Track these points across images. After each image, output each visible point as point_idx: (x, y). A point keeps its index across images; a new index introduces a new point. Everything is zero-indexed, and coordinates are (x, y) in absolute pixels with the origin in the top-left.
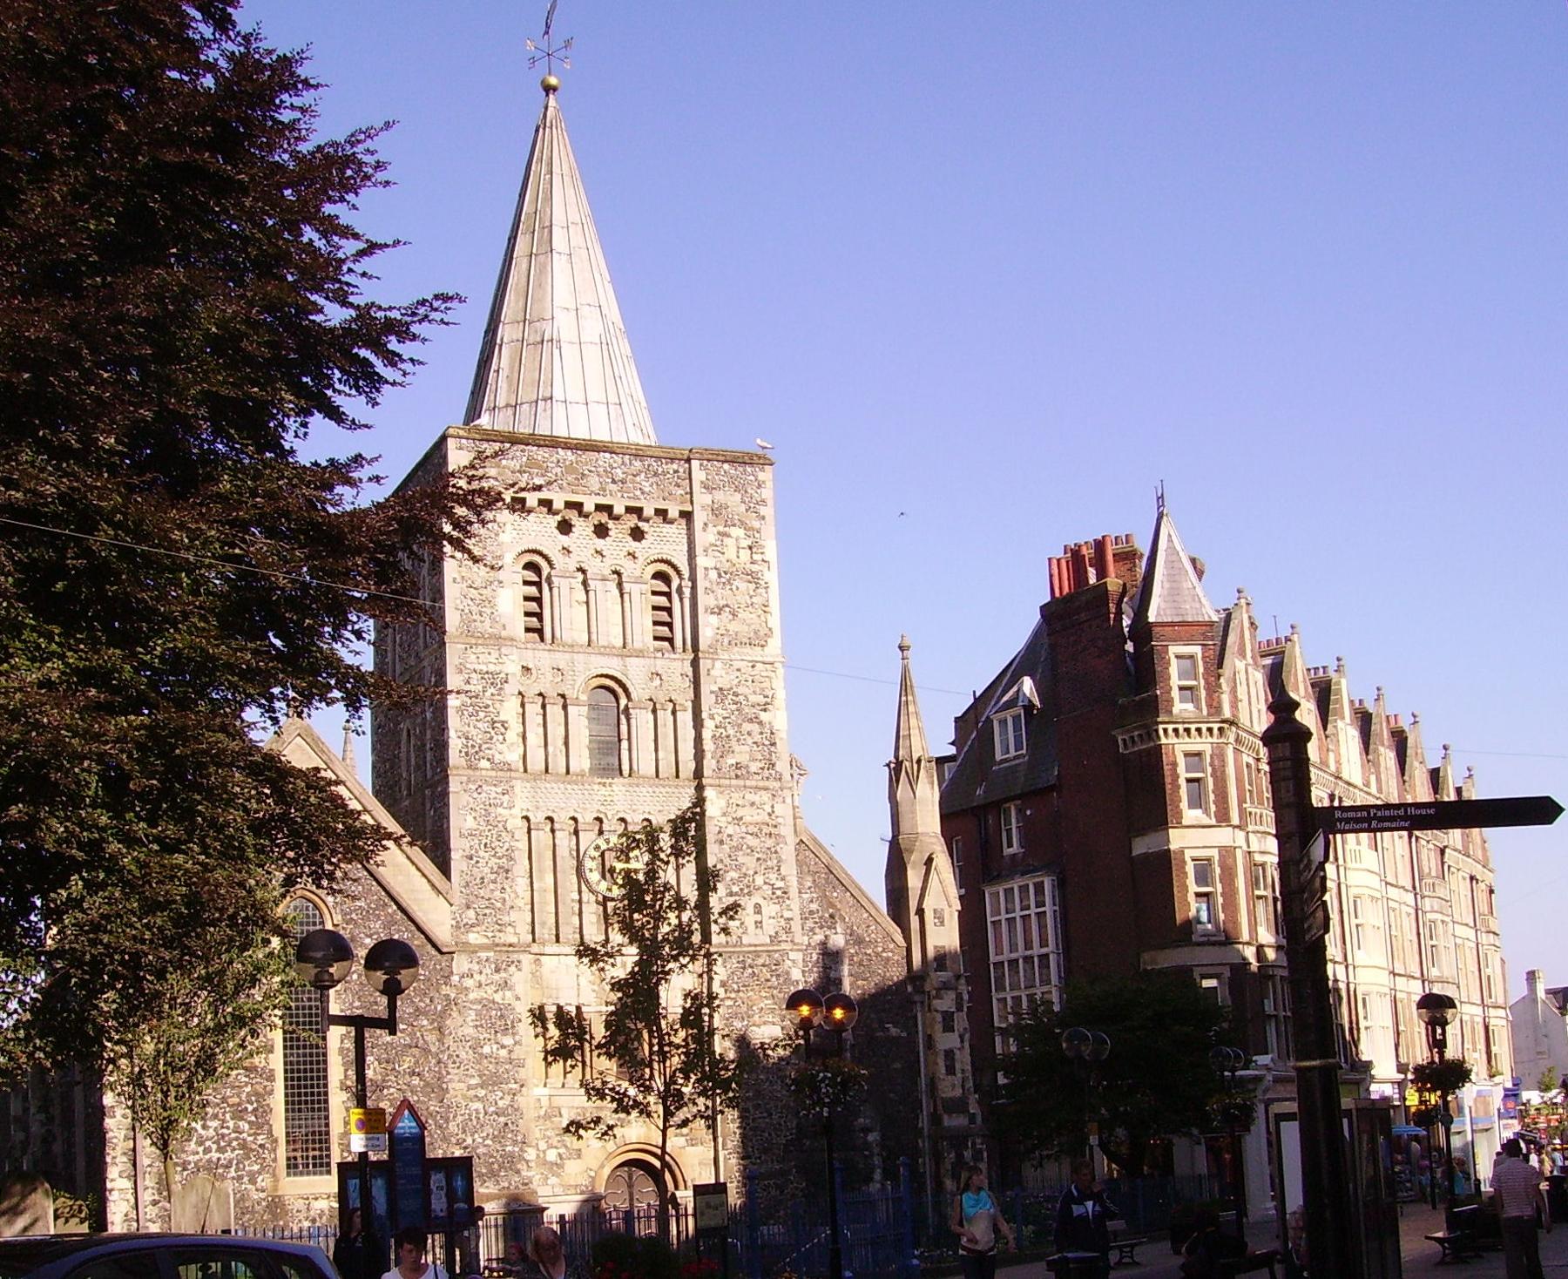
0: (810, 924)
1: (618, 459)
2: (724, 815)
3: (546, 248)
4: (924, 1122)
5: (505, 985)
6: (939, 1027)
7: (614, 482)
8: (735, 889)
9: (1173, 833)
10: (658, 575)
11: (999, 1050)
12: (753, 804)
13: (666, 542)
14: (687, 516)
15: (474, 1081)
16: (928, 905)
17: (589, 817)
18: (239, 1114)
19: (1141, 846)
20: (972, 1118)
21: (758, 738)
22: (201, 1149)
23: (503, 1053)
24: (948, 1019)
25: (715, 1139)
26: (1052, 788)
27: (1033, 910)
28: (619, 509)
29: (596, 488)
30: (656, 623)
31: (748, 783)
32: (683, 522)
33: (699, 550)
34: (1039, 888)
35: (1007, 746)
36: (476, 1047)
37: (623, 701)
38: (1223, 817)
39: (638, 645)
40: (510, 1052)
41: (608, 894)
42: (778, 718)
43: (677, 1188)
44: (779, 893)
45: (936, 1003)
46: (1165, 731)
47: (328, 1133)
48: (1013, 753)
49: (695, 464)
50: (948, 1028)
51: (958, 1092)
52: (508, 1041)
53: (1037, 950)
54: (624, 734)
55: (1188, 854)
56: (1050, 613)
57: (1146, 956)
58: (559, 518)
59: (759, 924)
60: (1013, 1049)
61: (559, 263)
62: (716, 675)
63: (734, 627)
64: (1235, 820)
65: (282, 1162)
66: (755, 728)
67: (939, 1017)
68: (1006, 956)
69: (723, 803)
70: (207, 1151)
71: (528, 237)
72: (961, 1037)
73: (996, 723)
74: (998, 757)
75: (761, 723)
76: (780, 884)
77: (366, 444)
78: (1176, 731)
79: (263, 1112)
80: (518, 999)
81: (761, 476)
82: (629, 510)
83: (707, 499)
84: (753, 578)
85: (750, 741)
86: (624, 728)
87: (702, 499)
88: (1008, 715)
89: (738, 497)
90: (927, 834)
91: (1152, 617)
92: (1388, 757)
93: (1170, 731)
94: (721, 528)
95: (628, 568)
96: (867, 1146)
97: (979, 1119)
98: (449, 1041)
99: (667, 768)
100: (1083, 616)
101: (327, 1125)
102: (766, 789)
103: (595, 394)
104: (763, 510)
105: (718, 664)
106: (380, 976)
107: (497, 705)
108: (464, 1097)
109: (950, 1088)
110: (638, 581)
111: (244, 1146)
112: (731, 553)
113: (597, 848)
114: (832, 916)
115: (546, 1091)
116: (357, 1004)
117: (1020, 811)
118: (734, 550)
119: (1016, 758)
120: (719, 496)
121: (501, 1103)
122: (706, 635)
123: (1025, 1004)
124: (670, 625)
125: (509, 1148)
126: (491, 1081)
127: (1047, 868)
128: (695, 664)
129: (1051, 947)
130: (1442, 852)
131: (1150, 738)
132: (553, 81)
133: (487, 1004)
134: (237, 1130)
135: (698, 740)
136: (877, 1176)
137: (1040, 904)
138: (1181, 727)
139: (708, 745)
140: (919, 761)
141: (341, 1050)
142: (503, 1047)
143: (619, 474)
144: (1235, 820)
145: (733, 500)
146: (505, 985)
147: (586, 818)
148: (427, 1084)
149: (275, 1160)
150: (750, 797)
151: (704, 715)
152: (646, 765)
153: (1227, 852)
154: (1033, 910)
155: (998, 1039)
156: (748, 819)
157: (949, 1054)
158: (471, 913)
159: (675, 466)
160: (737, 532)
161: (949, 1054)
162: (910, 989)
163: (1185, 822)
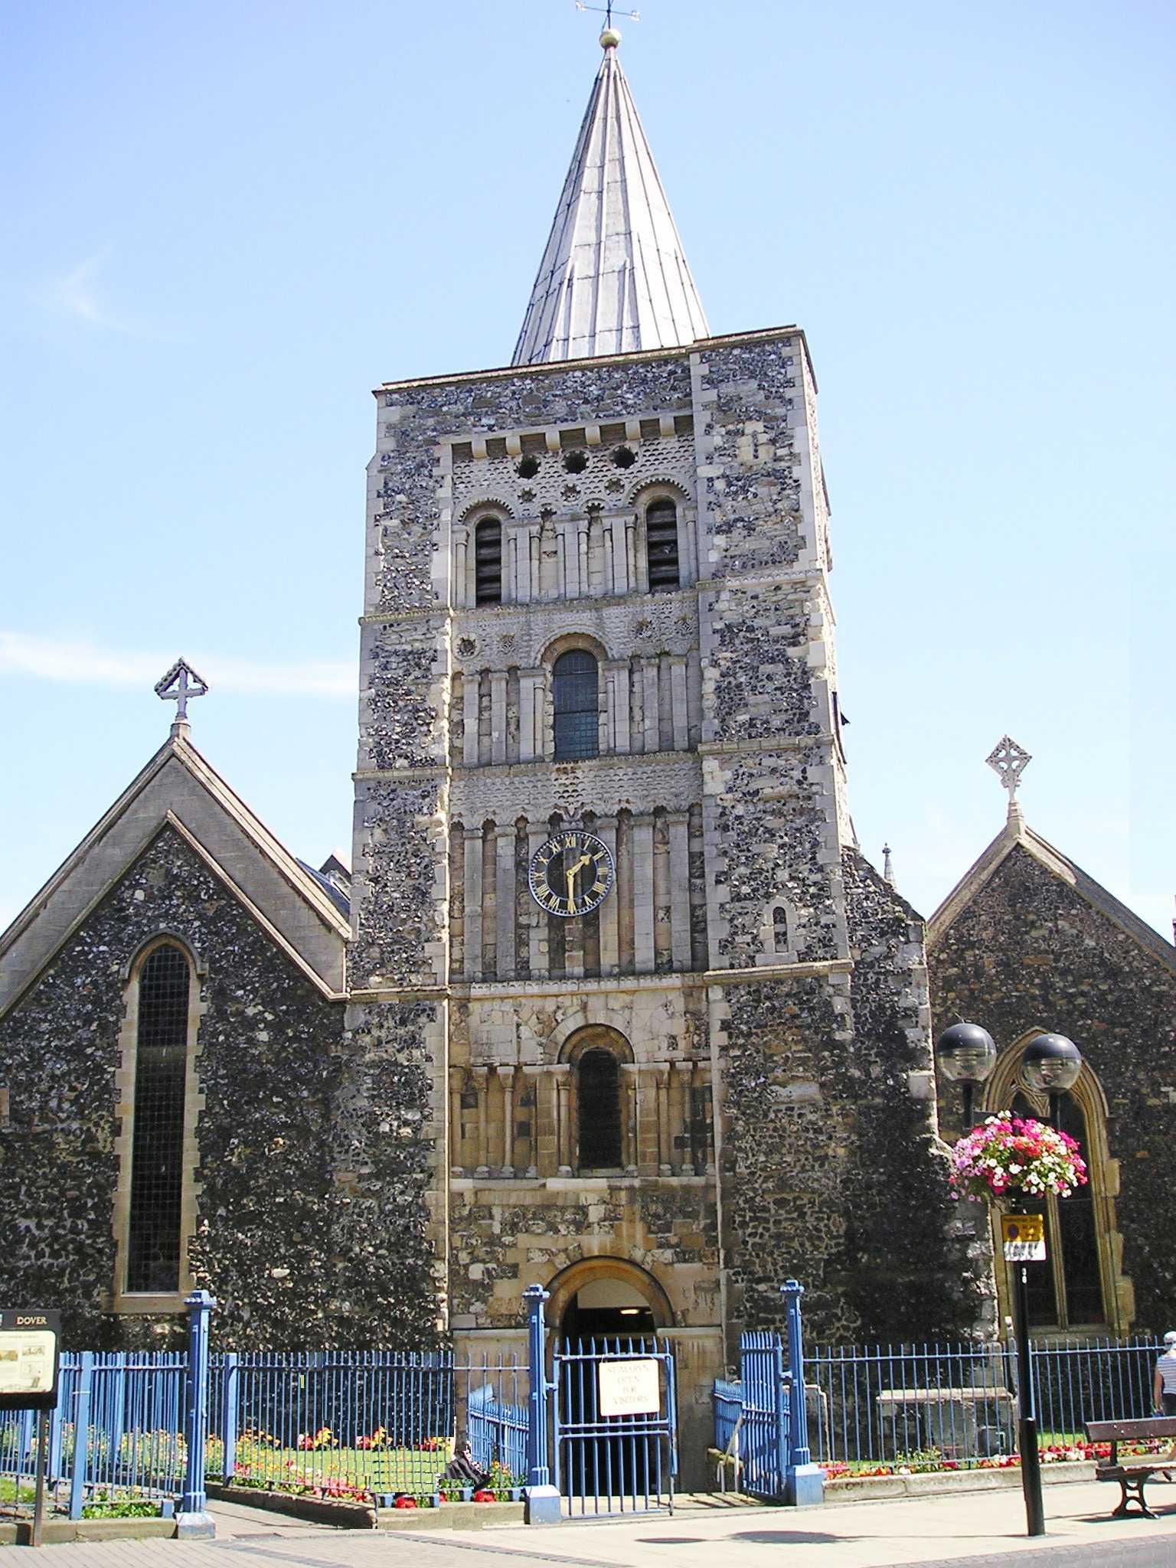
2: (730, 790)
5: (413, 1042)
7: (586, 402)
8: (745, 889)
12: (774, 770)
15: (365, 1170)
18: (78, 1212)
22: (33, 1254)
23: (406, 1131)
36: (373, 1121)
44: (812, 890)
59: (781, 937)
63: (748, 545)
66: (780, 668)
69: (729, 775)
70: (40, 1255)
75: (787, 661)
79: (105, 1207)
80: (429, 1059)
81: (786, 351)
83: (712, 395)
87: (703, 395)
89: (754, 384)
94: (731, 427)
98: (336, 1117)
104: (789, 393)
107: (423, 690)
108: (354, 1190)
112: (746, 453)
116: (222, 1072)
120: (728, 389)
125: (411, 1261)
126: (387, 1170)
131: (1085, 1196)
133: (388, 1067)
134: (74, 1230)
141: (199, 1132)
142: (406, 1123)
145: (748, 389)
146: (413, 1042)
147: (505, 818)
148: (304, 1174)
150: (768, 762)
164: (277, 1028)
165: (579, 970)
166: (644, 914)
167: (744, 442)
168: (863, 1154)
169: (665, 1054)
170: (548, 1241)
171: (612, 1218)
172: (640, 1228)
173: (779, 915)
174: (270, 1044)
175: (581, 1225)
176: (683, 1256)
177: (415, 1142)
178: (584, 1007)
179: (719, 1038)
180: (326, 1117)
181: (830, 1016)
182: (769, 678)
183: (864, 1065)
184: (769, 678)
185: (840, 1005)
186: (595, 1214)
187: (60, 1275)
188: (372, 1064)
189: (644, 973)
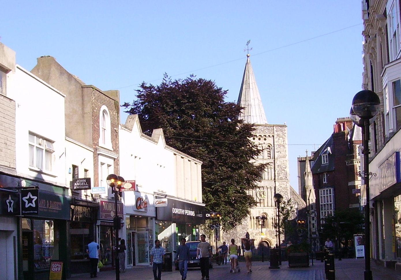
1: (262, 127)
2: (279, 186)
3: (248, 88)
4: (309, 236)
7: (262, 131)
9: (356, 182)
11: (321, 223)
13: (270, 141)
14: (273, 136)
19: (350, 184)
20: (317, 235)
21: (284, 173)
23: (245, 224)
24: (313, 218)
25: (277, 238)
26: (333, 171)
28: (262, 136)
29: (259, 132)
30: (268, 154)
31: (283, 181)
32: (272, 137)
33: (275, 142)
34: (330, 190)
35: (325, 161)
39: (265, 158)
40: (246, 224)
41: (261, 199)
42: (287, 170)
43: (271, 245)
45: (311, 215)
46: (355, 162)
47: (220, 236)
48: (325, 163)
49: (275, 127)
50: (313, 220)
51: (315, 231)
52: (246, 222)
53: (329, 203)
57: (350, 205)
60: (324, 223)
61: (251, 90)
62: (278, 163)
63: (280, 155)
65: (214, 240)
66: (284, 171)
67: (312, 218)
68: (323, 203)
71: (245, 85)
72: (315, 221)
73: (322, 157)
74: (323, 163)
75: (285, 171)
76: (287, 197)
77: (256, 161)
78: (357, 162)
81: (285, 129)
82: (264, 136)
83: (276, 133)
84: (284, 146)
85: (283, 173)
87: (276, 133)
88: (325, 155)
90: (310, 186)
91: (353, 140)
93: (356, 162)
94: (279, 138)
97: (318, 236)
99: (270, 178)
100: (340, 138)
101: (220, 235)
102: (285, 181)
103: (258, 114)
104: (285, 135)
109: (313, 230)
112: (280, 142)
113: (259, 191)
114: (296, 202)
115: (251, 230)
117: (326, 174)
118: (281, 142)
119: (326, 164)
120: (278, 133)
121: (245, 232)
124: (270, 154)
127: (331, 187)
129: (332, 202)
131: (352, 163)
132: (248, 55)
135: (275, 173)
137: (330, 193)
138: (358, 161)
139: (276, 174)
140: (309, 173)
143: (263, 130)
145: (280, 133)
149: (213, 240)
150: (283, 183)
151: (276, 170)
152: (266, 178)
154: (329, 195)
155: (321, 221)
156: (282, 186)
157: (313, 224)
159: (271, 128)
160: (281, 139)
161: (313, 224)
162: (307, 213)
163: (358, 180)
169: (272, 216)
172: (269, 235)
178: (263, 210)
182: (283, 172)
184: (283, 172)
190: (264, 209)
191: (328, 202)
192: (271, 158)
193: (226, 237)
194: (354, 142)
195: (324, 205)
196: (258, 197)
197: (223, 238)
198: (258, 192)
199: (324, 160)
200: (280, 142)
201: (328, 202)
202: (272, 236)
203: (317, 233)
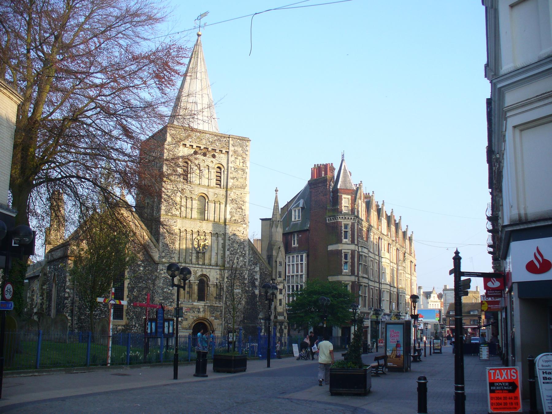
0: (251, 263)
6: (278, 293)
10: (219, 167)
14: (228, 152)
16: (278, 260)
17: (196, 230)
20: (285, 317)
21: (241, 213)
23: (169, 291)
24: (281, 290)
26: (307, 230)
27: (299, 262)
33: (230, 162)
34: (302, 256)
37: (207, 200)
38: (353, 242)
48: (297, 219)
49: (231, 139)
51: (282, 310)
53: (300, 273)
54: (206, 209)
55: (343, 251)
56: (310, 183)
58: (194, 150)
63: (237, 183)
64: (356, 243)
66: (241, 210)
68: (291, 274)
74: (293, 220)
76: (244, 252)
81: (247, 144)
86: (206, 207)
87: (232, 148)
89: (241, 149)
92: (393, 228)
95: (211, 165)
96: (261, 323)
98: (156, 287)
104: (247, 153)
105: (232, 193)
106: (170, 272)
110: (214, 168)
111: (101, 310)
112: (238, 163)
117: (298, 235)
120: (236, 148)
122: (230, 184)
123: (299, 287)
124: (220, 181)
128: (227, 191)
130: (405, 254)
132: (200, 33)
136: (263, 331)
141: (128, 287)
143: (211, 140)
144: (356, 243)
145: (239, 149)
147: (195, 230)
153: (353, 252)
154: (295, 263)
158: (164, 254)
160: (240, 158)
161: (280, 300)
163: (343, 242)
164: (144, 267)
165: (201, 263)
166: (214, 254)
167: (238, 161)
168: (247, 303)
170: (193, 314)
171: (204, 311)
172: (209, 313)
173: (238, 259)
174: (143, 270)
175: (199, 312)
176: (216, 319)
177: (171, 294)
178: (202, 271)
179: (226, 280)
180: (154, 287)
181: (244, 279)
183: (249, 288)
185: (246, 276)
186: (201, 310)
187: (96, 316)
188: (163, 277)
189: (213, 266)
190: (204, 270)
191: (297, 272)
192: (221, 188)
193: (134, 312)
194: (340, 191)
195: (293, 276)
196: (85, 107)
197: (128, 313)
198: (196, 240)
199: (295, 216)
200: (238, 163)
201: (297, 272)
202: (214, 315)
203: (285, 314)
